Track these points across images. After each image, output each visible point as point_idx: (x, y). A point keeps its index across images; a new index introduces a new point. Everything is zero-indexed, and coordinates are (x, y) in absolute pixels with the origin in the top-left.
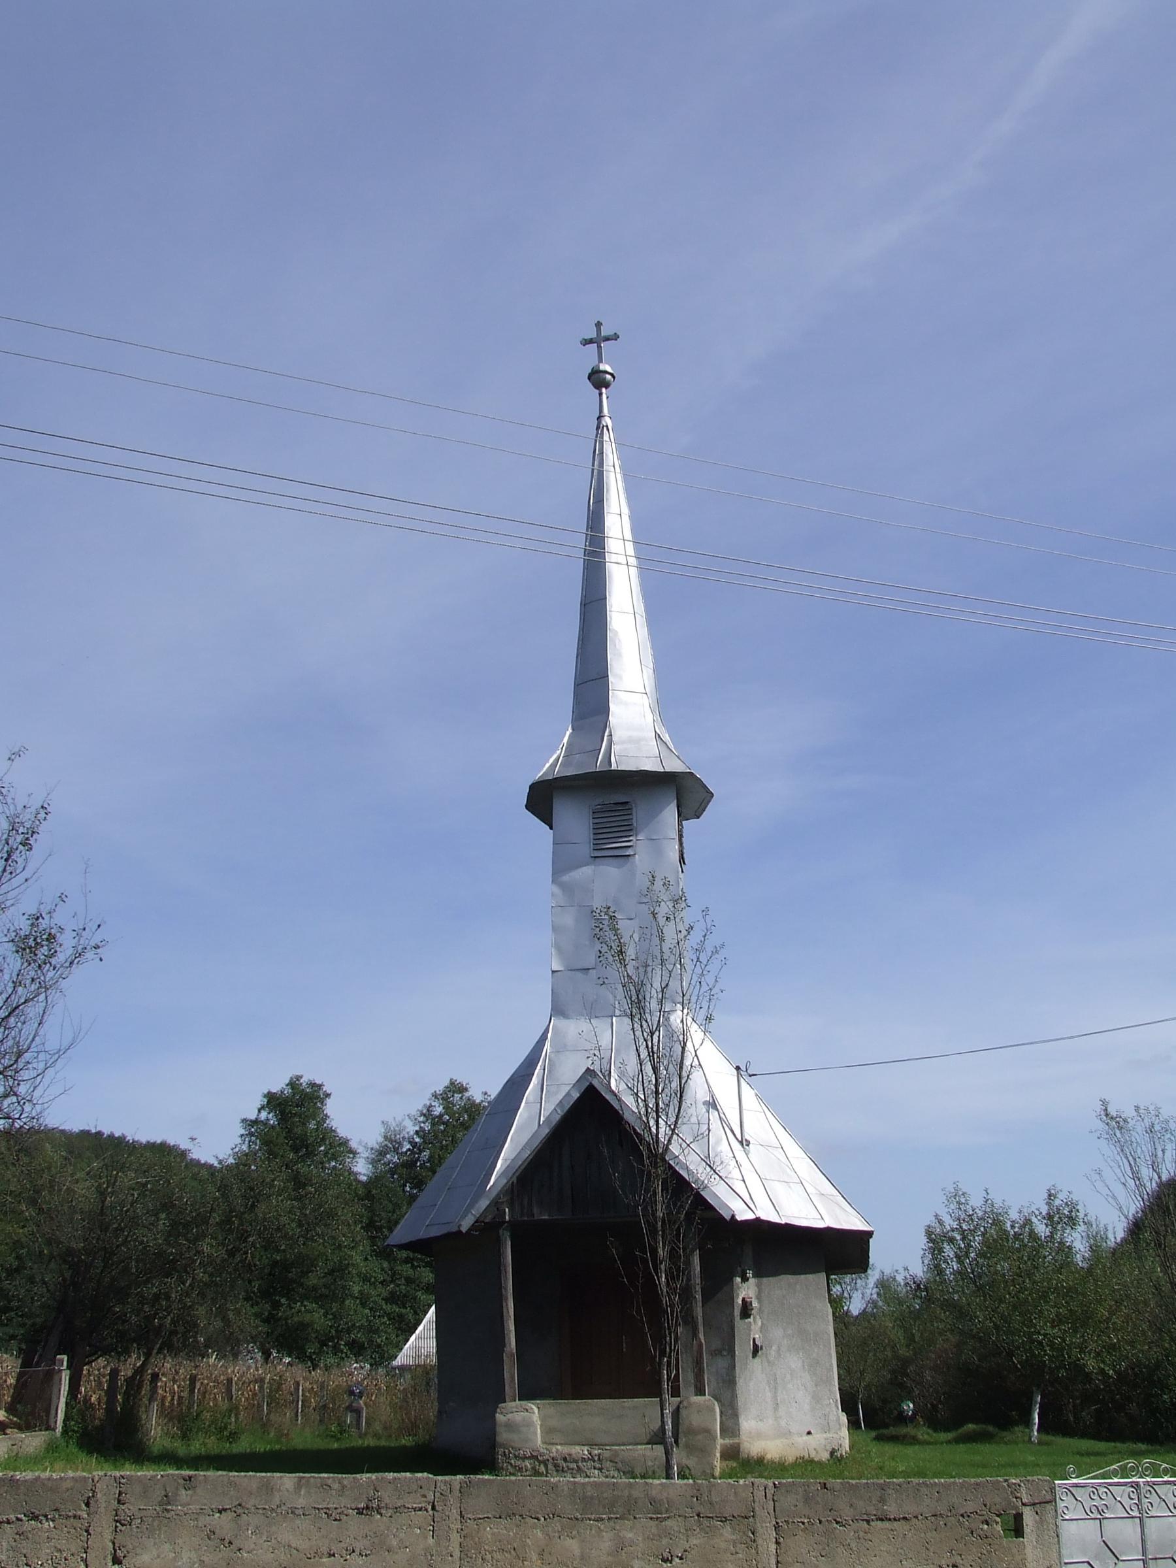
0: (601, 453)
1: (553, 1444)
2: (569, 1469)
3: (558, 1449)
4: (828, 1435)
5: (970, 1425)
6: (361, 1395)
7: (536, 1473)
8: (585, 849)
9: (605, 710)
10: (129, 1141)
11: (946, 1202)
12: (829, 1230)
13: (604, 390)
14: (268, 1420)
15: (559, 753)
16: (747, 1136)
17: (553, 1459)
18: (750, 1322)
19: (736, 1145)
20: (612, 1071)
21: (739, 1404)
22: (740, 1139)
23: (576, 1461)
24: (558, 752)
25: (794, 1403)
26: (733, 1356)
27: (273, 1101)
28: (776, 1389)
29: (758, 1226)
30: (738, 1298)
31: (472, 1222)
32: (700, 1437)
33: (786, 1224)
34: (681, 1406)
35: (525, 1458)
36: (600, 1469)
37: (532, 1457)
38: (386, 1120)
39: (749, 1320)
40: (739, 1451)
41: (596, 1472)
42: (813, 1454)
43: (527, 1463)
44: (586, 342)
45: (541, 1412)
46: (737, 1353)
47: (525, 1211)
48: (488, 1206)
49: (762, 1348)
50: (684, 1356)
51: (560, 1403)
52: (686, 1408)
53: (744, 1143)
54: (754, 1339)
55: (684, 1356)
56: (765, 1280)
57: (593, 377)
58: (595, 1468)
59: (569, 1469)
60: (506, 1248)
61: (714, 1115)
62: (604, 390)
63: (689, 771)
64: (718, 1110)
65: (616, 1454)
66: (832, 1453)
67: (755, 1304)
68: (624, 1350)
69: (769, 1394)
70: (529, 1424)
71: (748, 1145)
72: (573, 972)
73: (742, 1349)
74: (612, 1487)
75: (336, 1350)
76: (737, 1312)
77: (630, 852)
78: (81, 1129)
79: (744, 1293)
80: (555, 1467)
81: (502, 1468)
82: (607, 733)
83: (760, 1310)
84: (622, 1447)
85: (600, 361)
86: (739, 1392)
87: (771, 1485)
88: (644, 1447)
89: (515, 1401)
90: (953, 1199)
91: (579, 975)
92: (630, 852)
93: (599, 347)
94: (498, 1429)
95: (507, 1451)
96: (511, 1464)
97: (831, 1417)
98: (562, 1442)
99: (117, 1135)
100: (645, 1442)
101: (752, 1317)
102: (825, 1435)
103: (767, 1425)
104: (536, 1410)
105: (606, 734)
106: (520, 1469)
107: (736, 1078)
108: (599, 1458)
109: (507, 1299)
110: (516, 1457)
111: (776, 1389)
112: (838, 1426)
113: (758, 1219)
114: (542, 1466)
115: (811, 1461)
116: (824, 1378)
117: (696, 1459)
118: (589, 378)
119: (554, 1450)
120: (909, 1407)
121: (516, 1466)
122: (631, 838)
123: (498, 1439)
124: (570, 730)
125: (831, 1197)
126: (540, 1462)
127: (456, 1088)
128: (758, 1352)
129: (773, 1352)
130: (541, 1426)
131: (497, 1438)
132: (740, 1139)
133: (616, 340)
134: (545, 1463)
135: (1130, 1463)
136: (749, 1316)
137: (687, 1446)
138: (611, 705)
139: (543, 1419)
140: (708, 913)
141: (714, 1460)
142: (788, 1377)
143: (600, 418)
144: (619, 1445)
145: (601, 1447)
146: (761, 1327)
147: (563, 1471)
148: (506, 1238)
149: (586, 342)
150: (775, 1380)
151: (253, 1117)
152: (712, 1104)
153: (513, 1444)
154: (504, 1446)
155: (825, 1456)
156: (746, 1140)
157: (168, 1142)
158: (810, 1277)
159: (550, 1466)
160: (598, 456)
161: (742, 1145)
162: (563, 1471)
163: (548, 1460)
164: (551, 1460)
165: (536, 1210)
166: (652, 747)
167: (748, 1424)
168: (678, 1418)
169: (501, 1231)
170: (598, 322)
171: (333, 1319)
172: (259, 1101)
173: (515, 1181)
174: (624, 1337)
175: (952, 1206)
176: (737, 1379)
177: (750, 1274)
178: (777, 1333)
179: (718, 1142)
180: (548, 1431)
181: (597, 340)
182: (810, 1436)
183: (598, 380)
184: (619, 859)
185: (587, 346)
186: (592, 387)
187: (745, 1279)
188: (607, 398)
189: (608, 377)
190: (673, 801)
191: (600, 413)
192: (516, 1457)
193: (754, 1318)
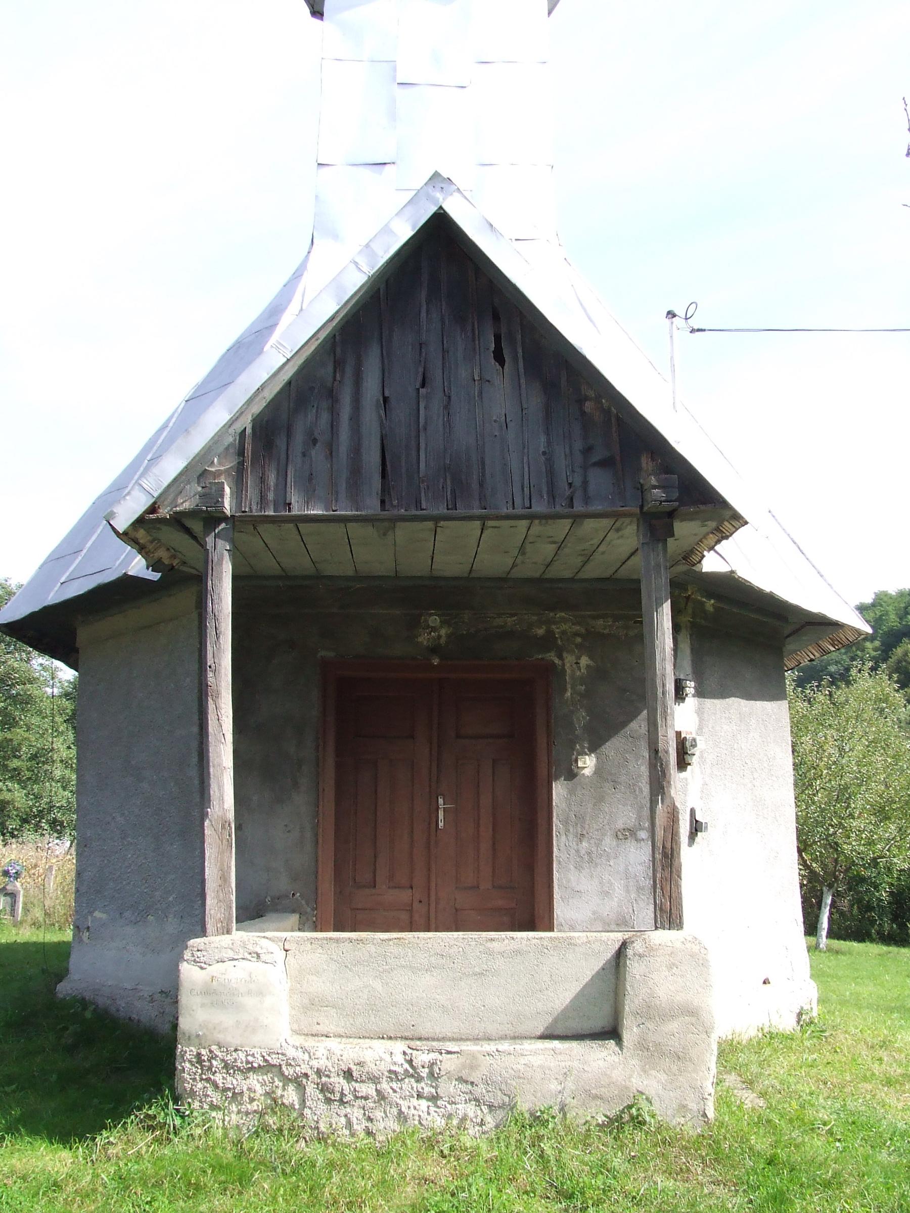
2: (357, 1098)
6: (17, 875)
17: (319, 1072)
23: (374, 1079)
32: (673, 1026)
36: (434, 1098)
37: (267, 1067)
41: (424, 1104)
43: (255, 1082)
47: (271, 496)
48: (181, 474)
50: (563, 838)
51: (337, 940)
52: (640, 956)
54: (693, 812)
55: (563, 838)
58: (419, 1096)
60: (220, 579)
68: (441, 824)
75: (37, 827)
80: (322, 1091)
81: (192, 1094)
91: (367, 172)
94: (185, 999)
95: (203, 1052)
96: (216, 1086)
98: (341, 1031)
100: (540, 1030)
106: (236, 1096)
108: (431, 1074)
109: (218, 695)
114: (291, 1088)
117: (663, 1077)
119: (321, 1052)
123: (185, 1023)
126: (286, 1080)
131: (182, 1021)
134: (298, 1082)
137: (642, 1046)
144: (476, 1039)
147: (341, 1101)
153: (220, 1037)
159: (311, 1089)
162: (341, 1101)
165: (294, 498)
171: (35, 799)
173: (249, 431)
174: (441, 801)
182: (422, 900)
192: (226, 1066)
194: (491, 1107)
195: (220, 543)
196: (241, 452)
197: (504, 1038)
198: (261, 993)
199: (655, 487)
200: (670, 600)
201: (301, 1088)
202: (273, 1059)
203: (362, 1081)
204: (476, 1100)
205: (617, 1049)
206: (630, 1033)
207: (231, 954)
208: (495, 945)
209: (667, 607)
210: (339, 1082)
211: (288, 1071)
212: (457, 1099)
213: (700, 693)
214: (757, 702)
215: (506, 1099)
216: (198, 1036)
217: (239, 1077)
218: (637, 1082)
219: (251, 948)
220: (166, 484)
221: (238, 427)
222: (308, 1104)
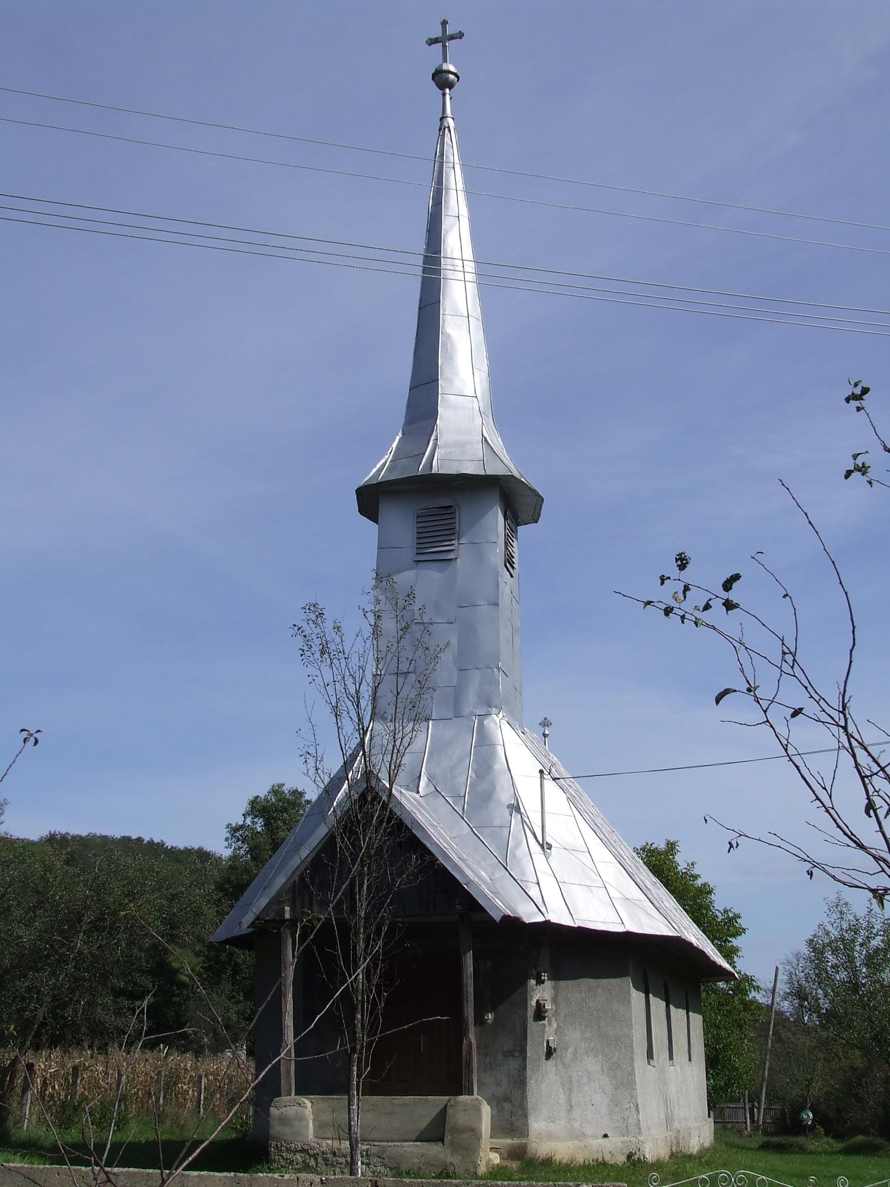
0: (442, 155)
1: (324, 1138)
2: (337, 1163)
3: (328, 1144)
4: (626, 1138)
5: (860, 1137)
7: (307, 1168)
8: (408, 553)
9: (434, 414)
10: (167, 847)
11: (828, 911)
12: (628, 934)
13: (447, 91)
14: (164, 1110)
15: (388, 457)
16: (548, 839)
17: (323, 1153)
18: (544, 1024)
19: (535, 848)
20: (422, 773)
21: (529, 1105)
22: (541, 842)
24: (386, 457)
25: (591, 1106)
26: (525, 1058)
27: (257, 808)
29: (548, 929)
30: (532, 999)
31: (252, 920)
32: (465, 1136)
33: (579, 928)
34: (448, 1104)
35: (296, 1151)
37: (303, 1151)
39: (544, 1022)
40: (525, 1152)
42: (607, 1158)
43: (298, 1157)
44: (432, 42)
45: (314, 1106)
46: (528, 1054)
49: (555, 1049)
51: (332, 1099)
52: (453, 1106)
53: (545, 847)
54: (548, 1042)
57: (435, 78)
59: (337, 1163)
61: (515, 819)
62: (447, 91)
63: (510, 474)
64: (521, 813)
65: (384, 1149)
66: (630, 1156)
67: (548, 1006)
68: (422, 1048)
69: (562, 1097)
70: (302, 1118)
71: (550, 848)
72: (391, 676)
73: (534, 1051)
74: (146, 1177)
76: (530, 1013)
77: (451, 556)
78: (123, 835)
79: (539, 995)
80: (324, 1161)
82: (433, 438)
83: (556, 1014)
84: (390, 1144)
85: (445, 60)
86: (529, 1094)
87: (319, 1180)
88: (412, 1143)
89: (290, 1095)
90: (835, 908)
92: (451, 556)
93: (444, 46)
95: (279, 1144)
97: (630, 1121)
99: (156, 842)
100: (414, 1138)
101: (547, 1019)
102: (622, 1139)
103: (559, 1127)
104: (309, 1104)
105: (433, 438)
106: (291, 1162)
107: (539, 779)
108: (367, 1154)
110: (287, 1150)
112: (638, 1131)
113: (547, 922)
114: (312, 1159)
115: (604, 1164)
116: (625, 1082)
117: (460, 1158)
118: (433, 79)
119: (324, 1144)
120: (808, 1116)
121: (287, 1159)
122: (453, 542)
123: (272, 1132)
124: (400, 435)
125: (637, 903)
126: (310, 1156)
128: (552, 1054)
130: (314, 1120)
132: (541, 842)
133: (461, 38)
134: (315, 1156)
135: (722, 1173)
136: (543, 1018)
137: (452, 1144)
138: (440, 410)
139: (316, 1113)
140: (425, 611)
141: (477, 1158)
142: (585, 1080)
143: (443, 119)
144: (388, 1141)
145: (370, 1143)
146: (556, 1030)
147: (332, 1165)
148: (287, 936)
149: (432, 42)
150: (570, 1082)
151: (241, 823)
152: (516, 808)
154: (277, 1139)
155: (621, 1159)
156: (547, 843)
157: (205, 849)
158: (613, 981)
160: (440, 159)
161: (543, 848)
163: (318, 1154)
164: (321, 1154)
166: (478, 449)
167: (537, 1125)
168: (446, 1114)
169: (282, 929)
170: (444, 20)
172: (244, 807)
173: (297, 881)
174: (422, 1036)
175: (835, 916)
176: (527, 1080)
177: (545, 976)
178: (574, 1035)
179: (518, 845)
180: (320, 1126)
181: (442, 40)
183: (442, 80)
184: (441, 563)
185: (432, 45)
186: (435, 85)
187: (540, 982)
188: (451, 99)
189: (451, 77)
190: (496, 504)
191: (443, 114)
193: (548, 1021)
194: (390, 1169)
195: (286, 930)
196: (294, 891)
197: (399, 1141)
198: (301, 1120)
199: (457, 904)
200: (471, 951)
201: (316, 1160)
202: (305, 1147)
203: (340, 1157)
204: (385, 1165)
205: (442, 1145)
206: (448, 1138)
207: (289, 1104)
208: (396, 1101)
209: (470, 956)
210: (330, 1156)
211: (311, 1152)
212: (377, 1165)
213: (554, 977)
214: (604, 980)
215: (396, 1165)
216: (276, 1137)
217: (292, 1154)
218: (449, 1159)
219: (297, 1101)
220: (261, 909)
221: (292, 881)
222: (319, 1165)
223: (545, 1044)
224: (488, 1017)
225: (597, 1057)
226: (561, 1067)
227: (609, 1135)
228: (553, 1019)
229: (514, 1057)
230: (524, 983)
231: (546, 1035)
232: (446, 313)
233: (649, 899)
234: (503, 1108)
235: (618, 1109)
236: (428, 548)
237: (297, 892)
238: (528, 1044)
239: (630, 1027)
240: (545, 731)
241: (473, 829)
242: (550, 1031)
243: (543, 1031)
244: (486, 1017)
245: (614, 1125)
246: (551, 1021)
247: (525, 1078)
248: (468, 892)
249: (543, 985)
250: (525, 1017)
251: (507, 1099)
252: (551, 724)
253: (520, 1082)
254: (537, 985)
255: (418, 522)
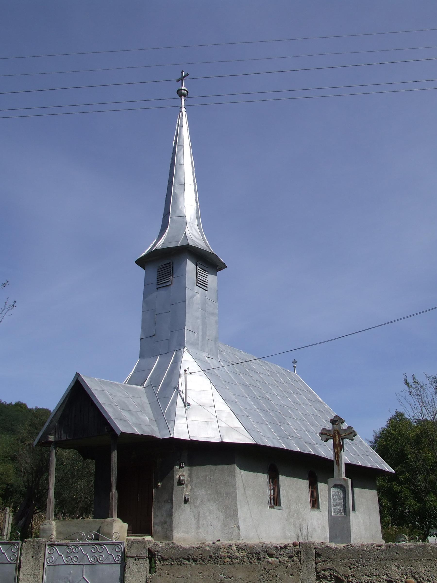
18: (183, 487)
21: (174, 525)
28: (198, 518)
38: (375, 430)
56: (195, 468)
69: (194, 522)
70: (50, 530)
73: (177, 498)
76: (175, 482)
79: (180, 474)
111: (198, 518)
112: (238, 538)
118: (177, 93)
122: (170, 278)
127: (399, 415)
129: (198, 502)
133: (188, 76)
139: (57, 527)
142: (208, 513)
158: (225, 466)
178: (201, 493)
180: (58, 533)
187: (181, 467)
223: (184, 497)
224: (159, 484)
225: (215, 502)
226: (193, 507)
227: (220, 540)
228: (189, 485)
229: (168, 503)
230: (172, 468)
231: (184, 492)
232: (175, 184)
233: (244, 427)
234: (164, 527)
235: (227, 528)
236: (161, 281)
237: (57, 429)
238: (174, 496)
239: (235, 488)
240: (294, 365)
241: (158, 399)
242: (187, 491)
243: (183, 490)
244: (158, 485)
245: (224, 535)
246: (188, 486)
247: (172, 512)
248: (109, 423)
249: (183, 469)
250: (173, 484)
251: (165, 523)
252: (297, 362)
253: (170, 515)
254: (179, 469)
255: (158, 272)
